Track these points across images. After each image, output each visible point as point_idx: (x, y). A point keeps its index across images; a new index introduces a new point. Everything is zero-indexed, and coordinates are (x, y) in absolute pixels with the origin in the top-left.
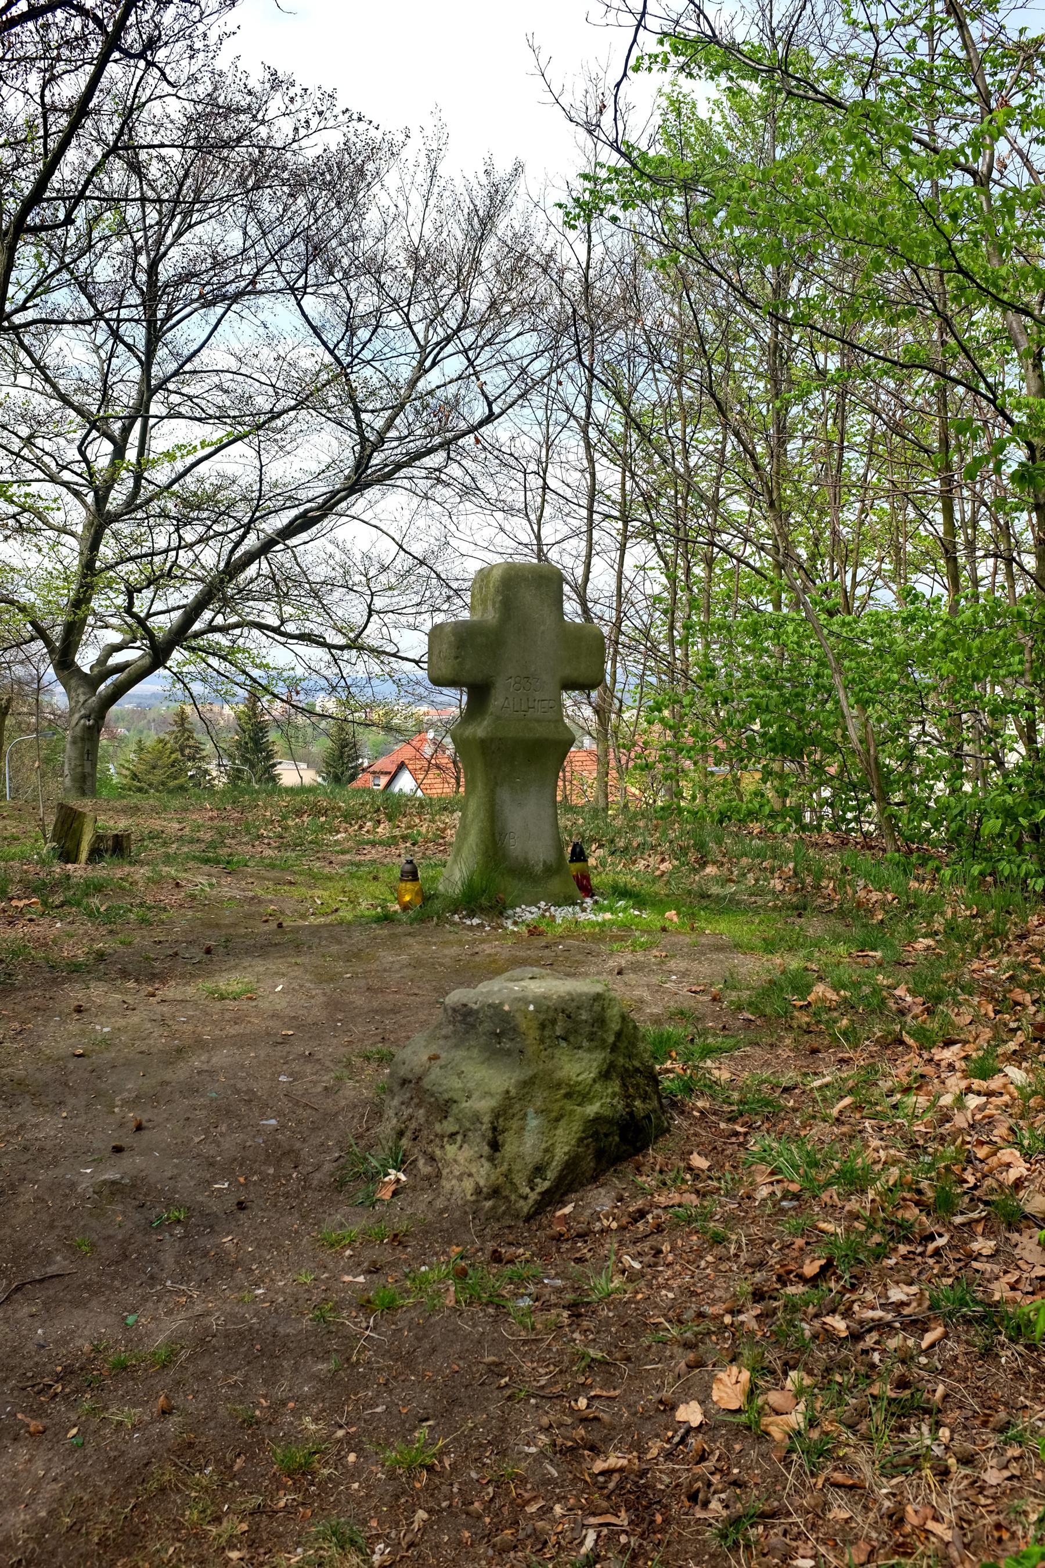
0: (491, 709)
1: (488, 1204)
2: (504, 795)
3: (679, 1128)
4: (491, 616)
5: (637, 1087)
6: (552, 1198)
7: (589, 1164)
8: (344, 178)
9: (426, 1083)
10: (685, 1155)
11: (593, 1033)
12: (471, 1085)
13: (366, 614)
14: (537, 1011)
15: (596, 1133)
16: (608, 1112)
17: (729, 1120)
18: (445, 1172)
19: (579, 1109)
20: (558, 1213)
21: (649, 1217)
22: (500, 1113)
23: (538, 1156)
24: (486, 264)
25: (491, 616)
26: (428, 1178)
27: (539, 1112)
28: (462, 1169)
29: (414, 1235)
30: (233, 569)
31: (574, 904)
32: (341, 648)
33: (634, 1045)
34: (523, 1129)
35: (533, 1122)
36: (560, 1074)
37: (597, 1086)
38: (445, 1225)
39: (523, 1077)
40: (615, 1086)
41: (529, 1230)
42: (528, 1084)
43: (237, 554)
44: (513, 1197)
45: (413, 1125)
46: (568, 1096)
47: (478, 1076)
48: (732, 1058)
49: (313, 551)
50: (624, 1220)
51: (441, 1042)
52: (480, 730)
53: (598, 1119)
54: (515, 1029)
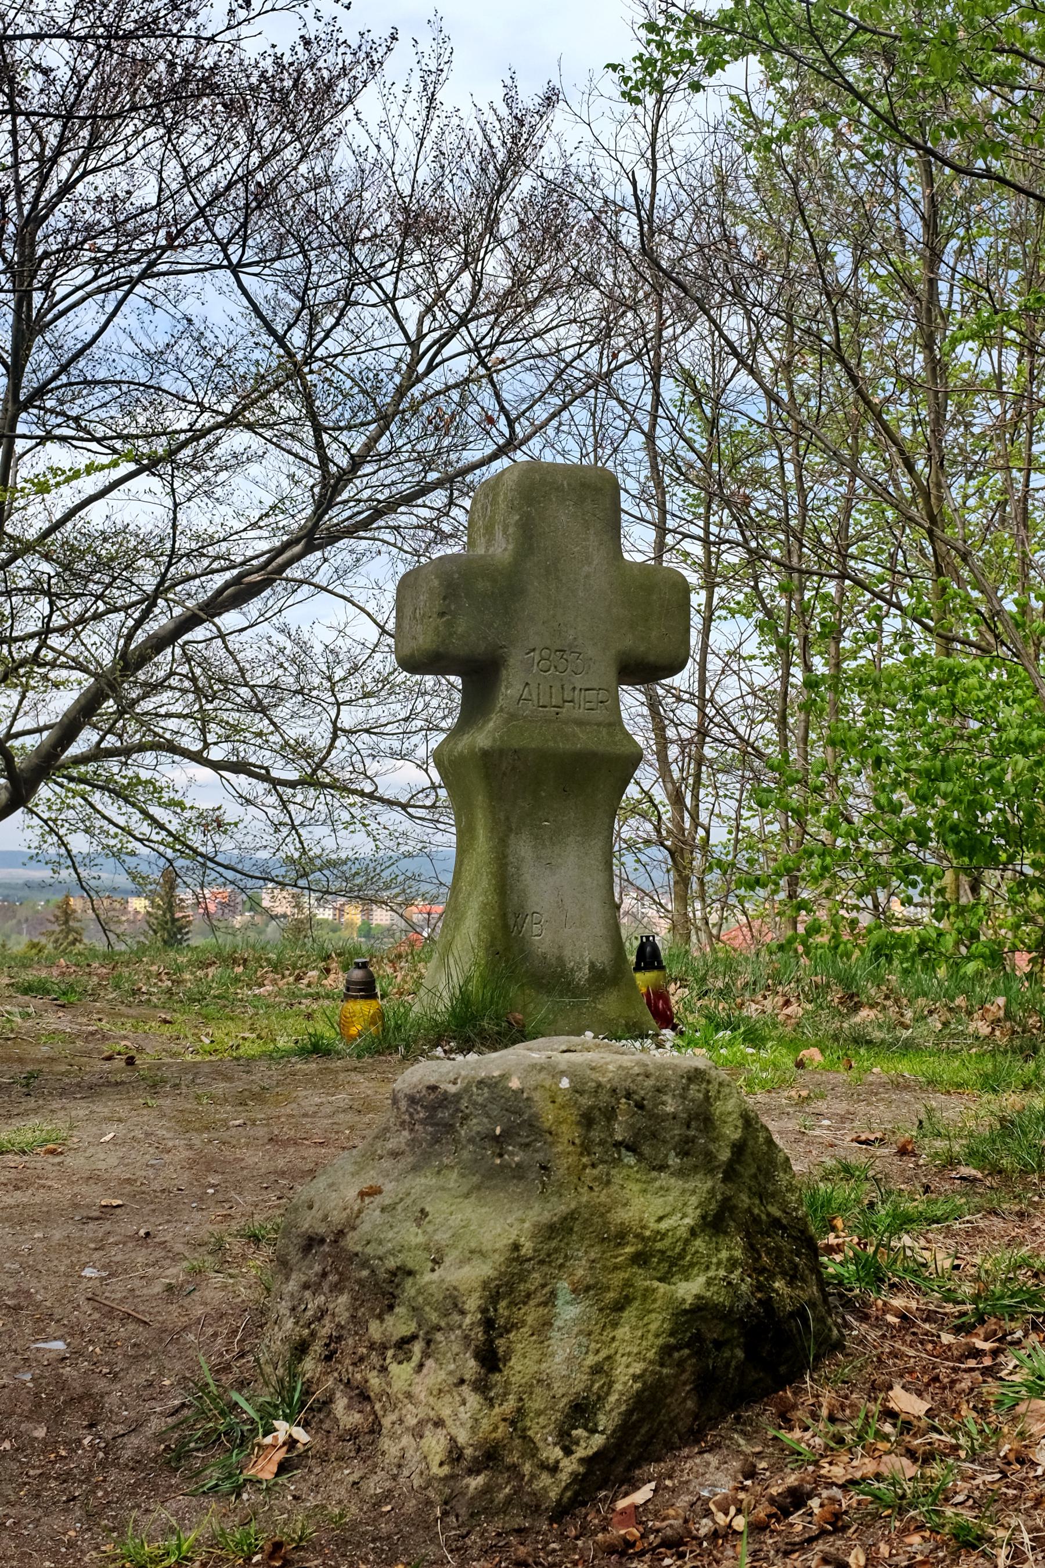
0: (501, 702)
1: (475, 1482)
2: (523, 848)
3: (861, 1341)
4: (501, 549)
5: (777, 1253)
6: (609, 1471)
7: (683, 1403)
8: (304, 98)
9: (352, 1242)
10: (878, 1389)
11: (688, 1140)
12: (442, 1237)
13: (328, 735)
14: (577, 1090)
15: (698, 1337)
16: (722, 1298)
17: (957, 1330)
18: (386, 1422)
19: (662, 1287)
20: (622, 1504)
21: (814, 1503)
22: (504, 1290)
23: (580, 1381)
24: (505, 228)
25: (501, 549)
26: (353, 1435)
27: (581, 1290)
28: (422, 1412)
29: (316, 1548)
30: (130, 662)
31: (643, 1036)
32: (292, 784)
33: (769, 1177)
34: (547, 1324)
35: (569, 1312)
36: (621, 1216)
37: (699, 1244)
38: (385, 1528)
39: (546, 1217)
40: (734, 1248)
41: (562, 1537)
42: (557, 1231)
43: (140, 637)
44: (527, 1468)
45: (326, 1329)
46: (640, 1259)
47: (456, 1220)
48: (949, 1233)
49: (249, 635)
50: (762, 1512)
51: (387, 1164)
52: (482, 738)
53: (701, 1309)
54: (532, 1125)
